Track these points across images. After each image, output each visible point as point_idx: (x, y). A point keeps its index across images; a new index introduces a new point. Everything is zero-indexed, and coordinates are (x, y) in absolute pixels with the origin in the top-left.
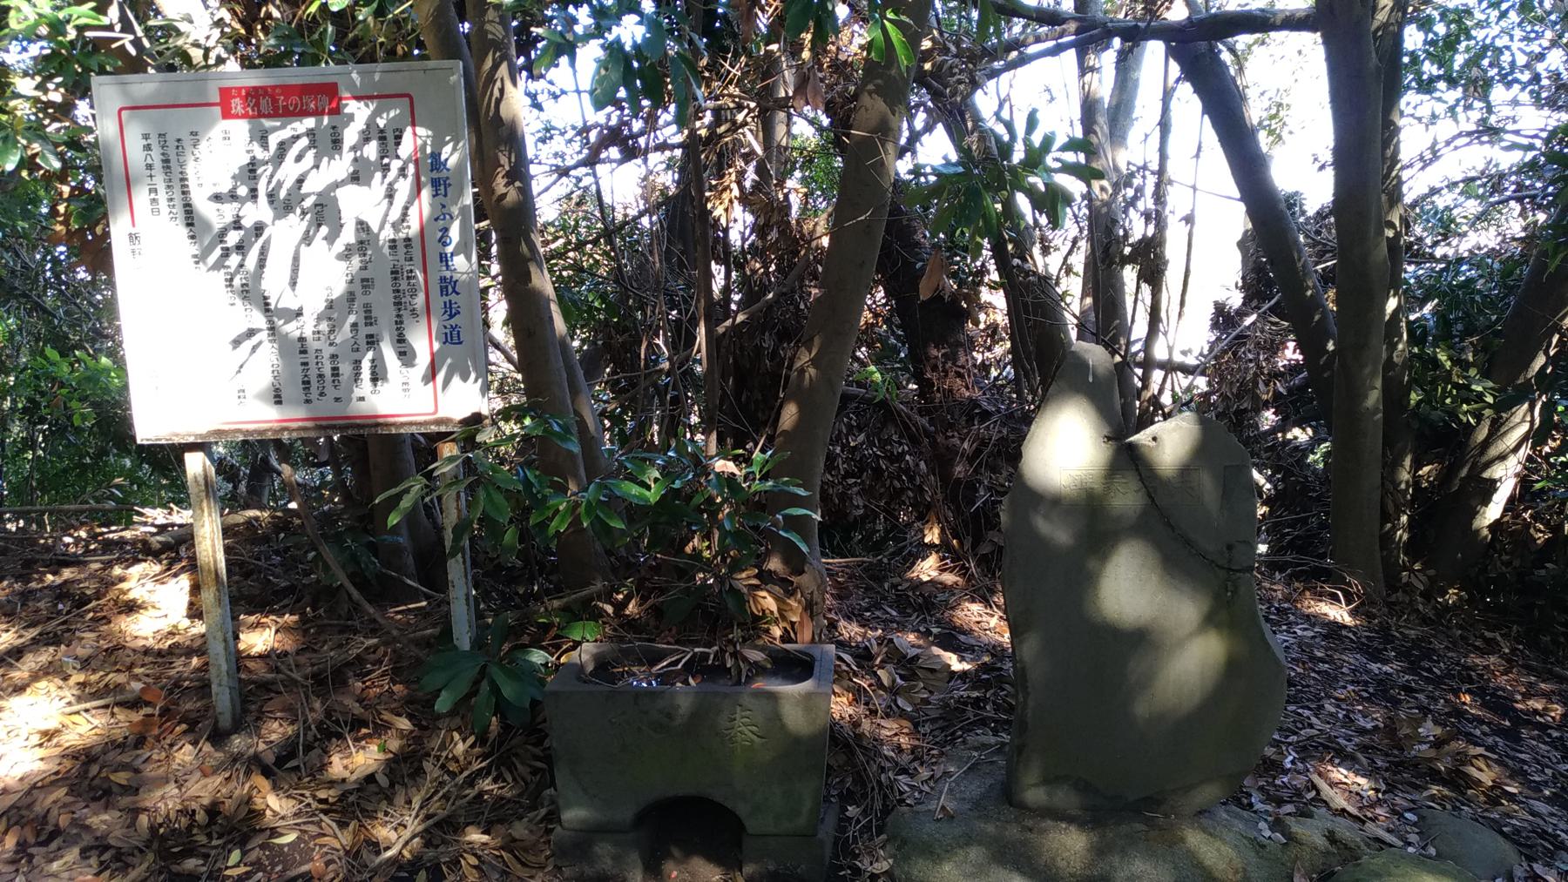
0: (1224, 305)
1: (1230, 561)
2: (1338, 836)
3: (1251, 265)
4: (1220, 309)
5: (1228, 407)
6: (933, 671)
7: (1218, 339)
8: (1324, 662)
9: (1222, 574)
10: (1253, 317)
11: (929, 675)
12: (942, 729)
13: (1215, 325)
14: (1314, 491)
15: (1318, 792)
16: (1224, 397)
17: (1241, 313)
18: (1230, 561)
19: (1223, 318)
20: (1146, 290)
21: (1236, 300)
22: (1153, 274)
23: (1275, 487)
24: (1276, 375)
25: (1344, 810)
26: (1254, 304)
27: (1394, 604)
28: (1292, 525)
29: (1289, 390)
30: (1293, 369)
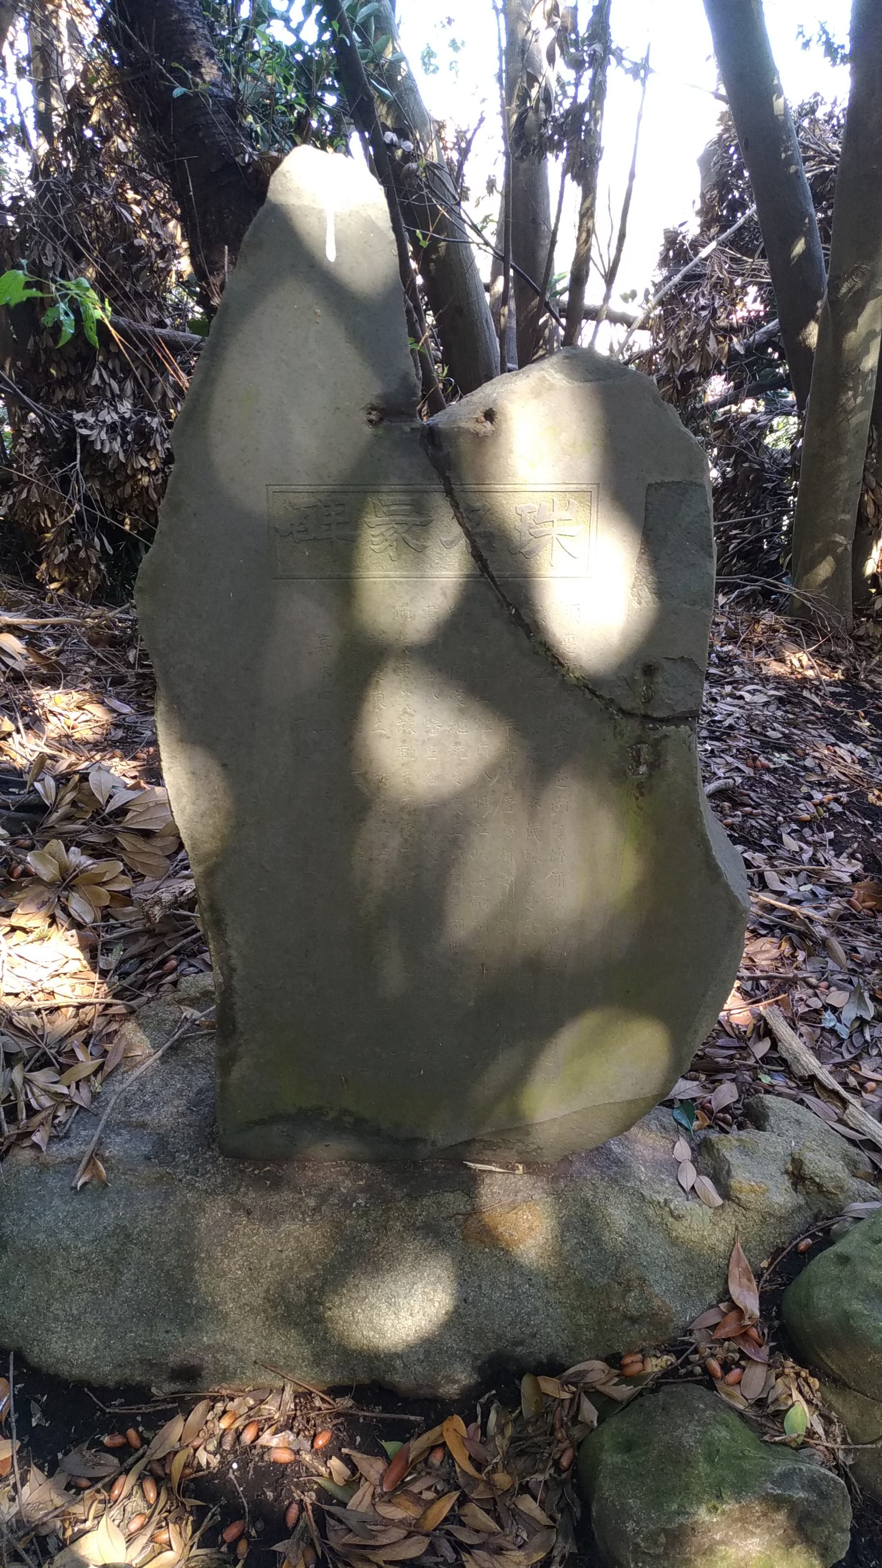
0: (677, 234)
1: (648, 700)
2: (809, 1168)
3: (714, 179)
4: (672, 239)
5: (672, 369)
6: (147, 834)
7: (667, 279)
8: (781, 750)
9: (630, 728)
10: (713, 245)
11: (141, 844)
12: (143, 957)
13: (664, 261)
14: (770, 480)
15: (774, 1046)
16: (669, 356)
17: (696, 245)
18: (648, 700)
19: (676, 252)
20: (574, 191)
21: (692, 229)
22: (583, 169)
23: (723, 474)
24: (731, 331)
25: (813, 1078)
26: (714, 231)
27: (860, 638)
28: (741, 526)
29: (748, 348)
30: (754, 323)
